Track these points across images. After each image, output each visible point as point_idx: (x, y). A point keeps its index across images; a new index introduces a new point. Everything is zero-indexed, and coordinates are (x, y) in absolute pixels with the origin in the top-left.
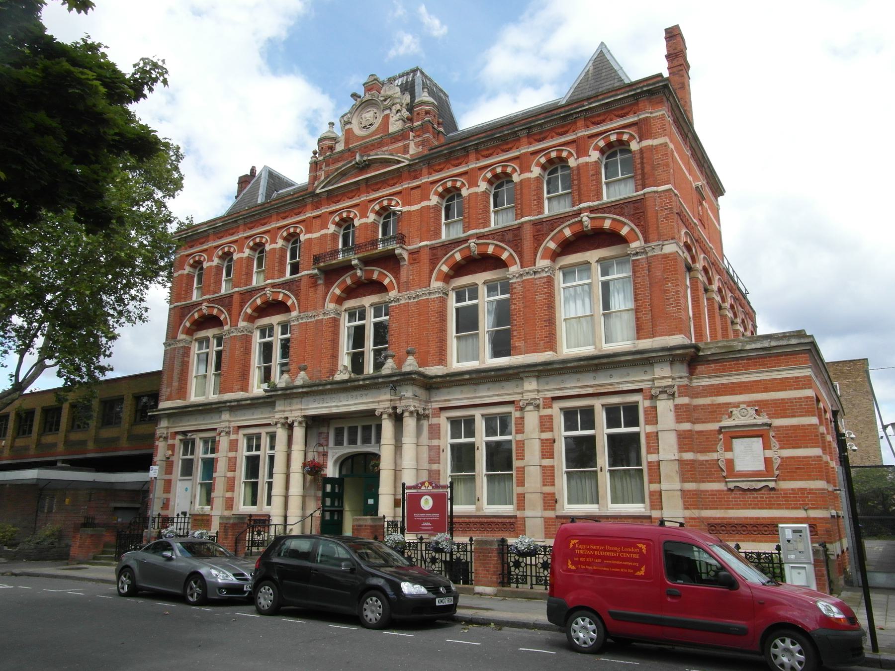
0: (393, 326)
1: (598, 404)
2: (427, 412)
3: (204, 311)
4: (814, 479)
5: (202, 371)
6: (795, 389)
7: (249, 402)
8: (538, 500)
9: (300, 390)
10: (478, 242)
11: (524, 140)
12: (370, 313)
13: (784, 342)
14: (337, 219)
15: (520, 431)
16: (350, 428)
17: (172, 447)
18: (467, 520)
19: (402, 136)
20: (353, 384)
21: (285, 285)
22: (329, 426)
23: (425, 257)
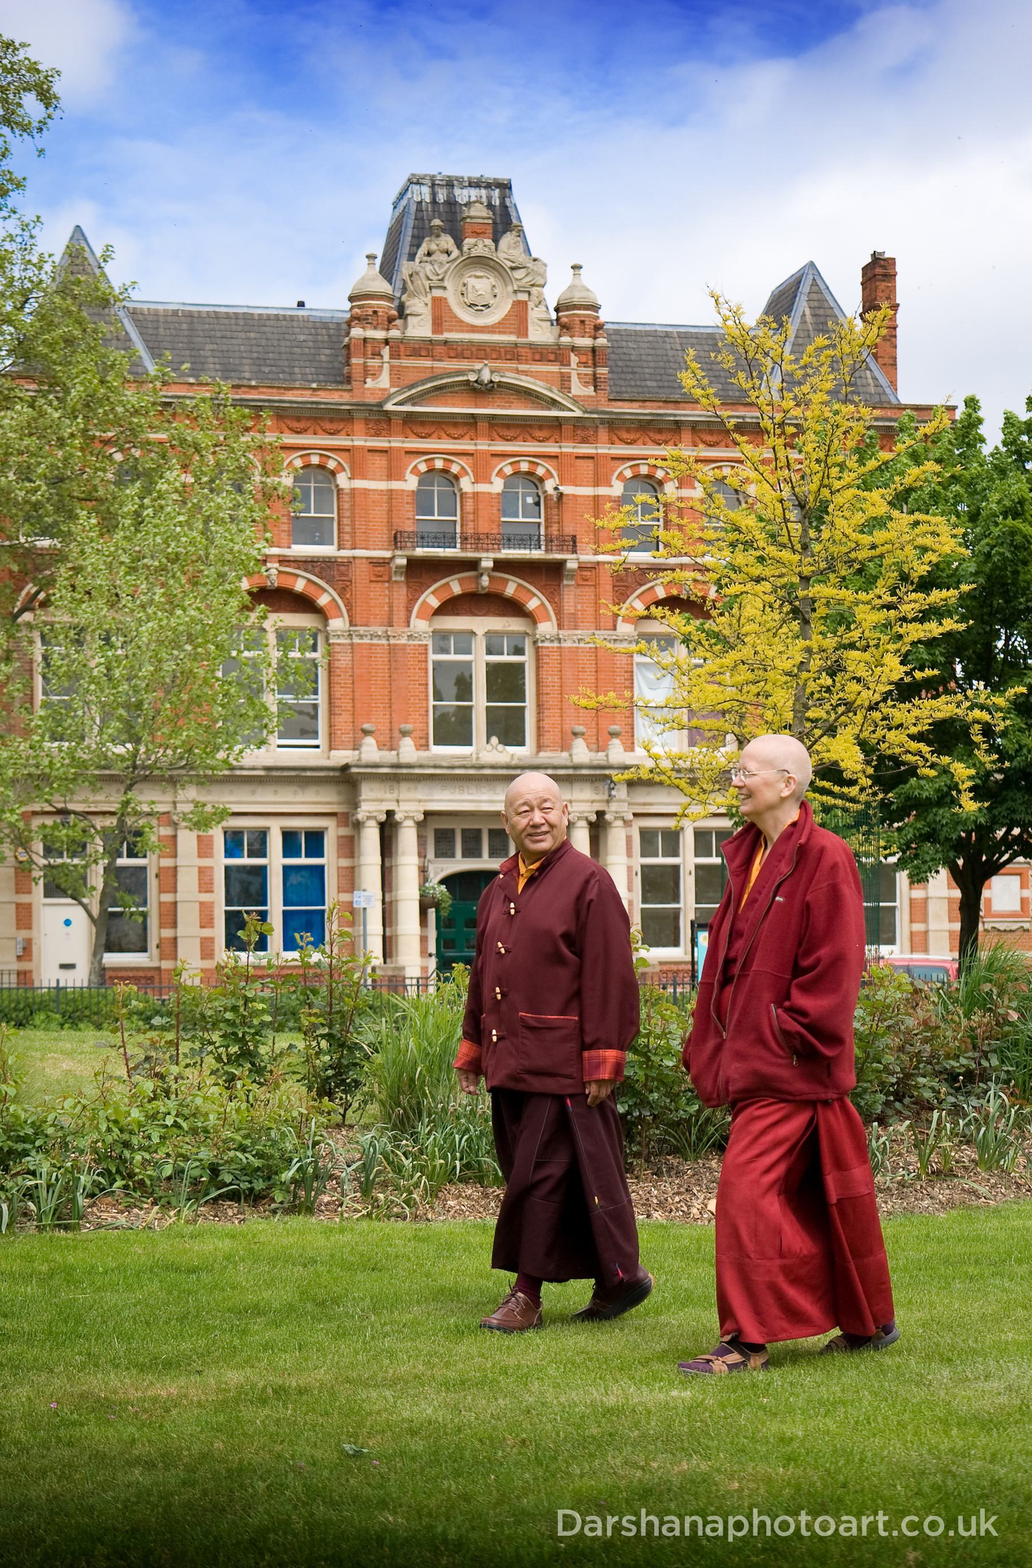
10: (282, 569)
11: (359, 426)
18: (675, 968)
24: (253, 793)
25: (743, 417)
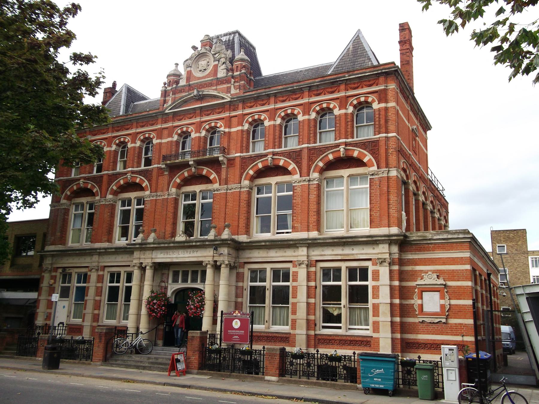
0: (216, 207)
1: (344, 266)
2: (236, 265)
3: (82, 185)
4: (467, 319)
5: (78, 226)
6: (461, 264)
7: (113, 250)
8: (304, 323)
9: (152, 246)
12: (199, 196)
13: (455, 236)
14: (117, 142)
15: (295, 280)
16: (183, 271)
17: (54, 278)
19: (225, 81)
20: (188, 244)
21: (140, 173)
22: (169, 270)
23: (238, 162)
24: (73, 259)
25: (293, 87)
